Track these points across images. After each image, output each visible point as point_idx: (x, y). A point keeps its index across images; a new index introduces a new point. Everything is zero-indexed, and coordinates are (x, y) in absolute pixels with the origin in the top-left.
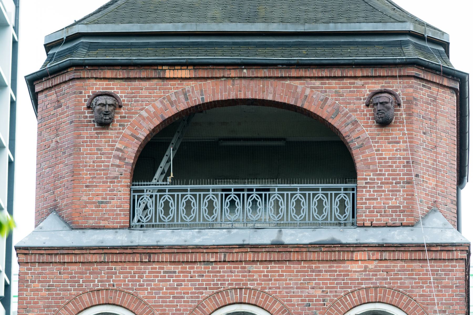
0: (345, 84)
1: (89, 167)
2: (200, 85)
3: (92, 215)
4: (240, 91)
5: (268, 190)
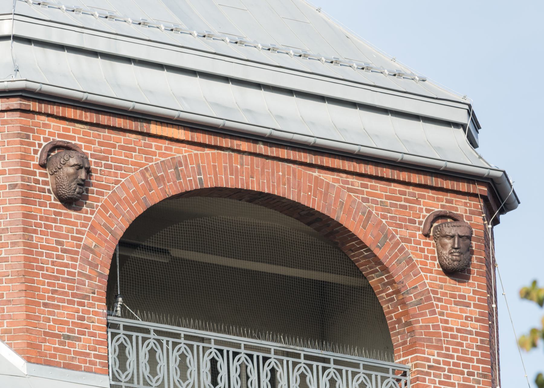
0: (393, 191)
1: (47, 271)
2: (196, 155)
3: (55, 356)
4: (252, 177)
5: (202, 340)
